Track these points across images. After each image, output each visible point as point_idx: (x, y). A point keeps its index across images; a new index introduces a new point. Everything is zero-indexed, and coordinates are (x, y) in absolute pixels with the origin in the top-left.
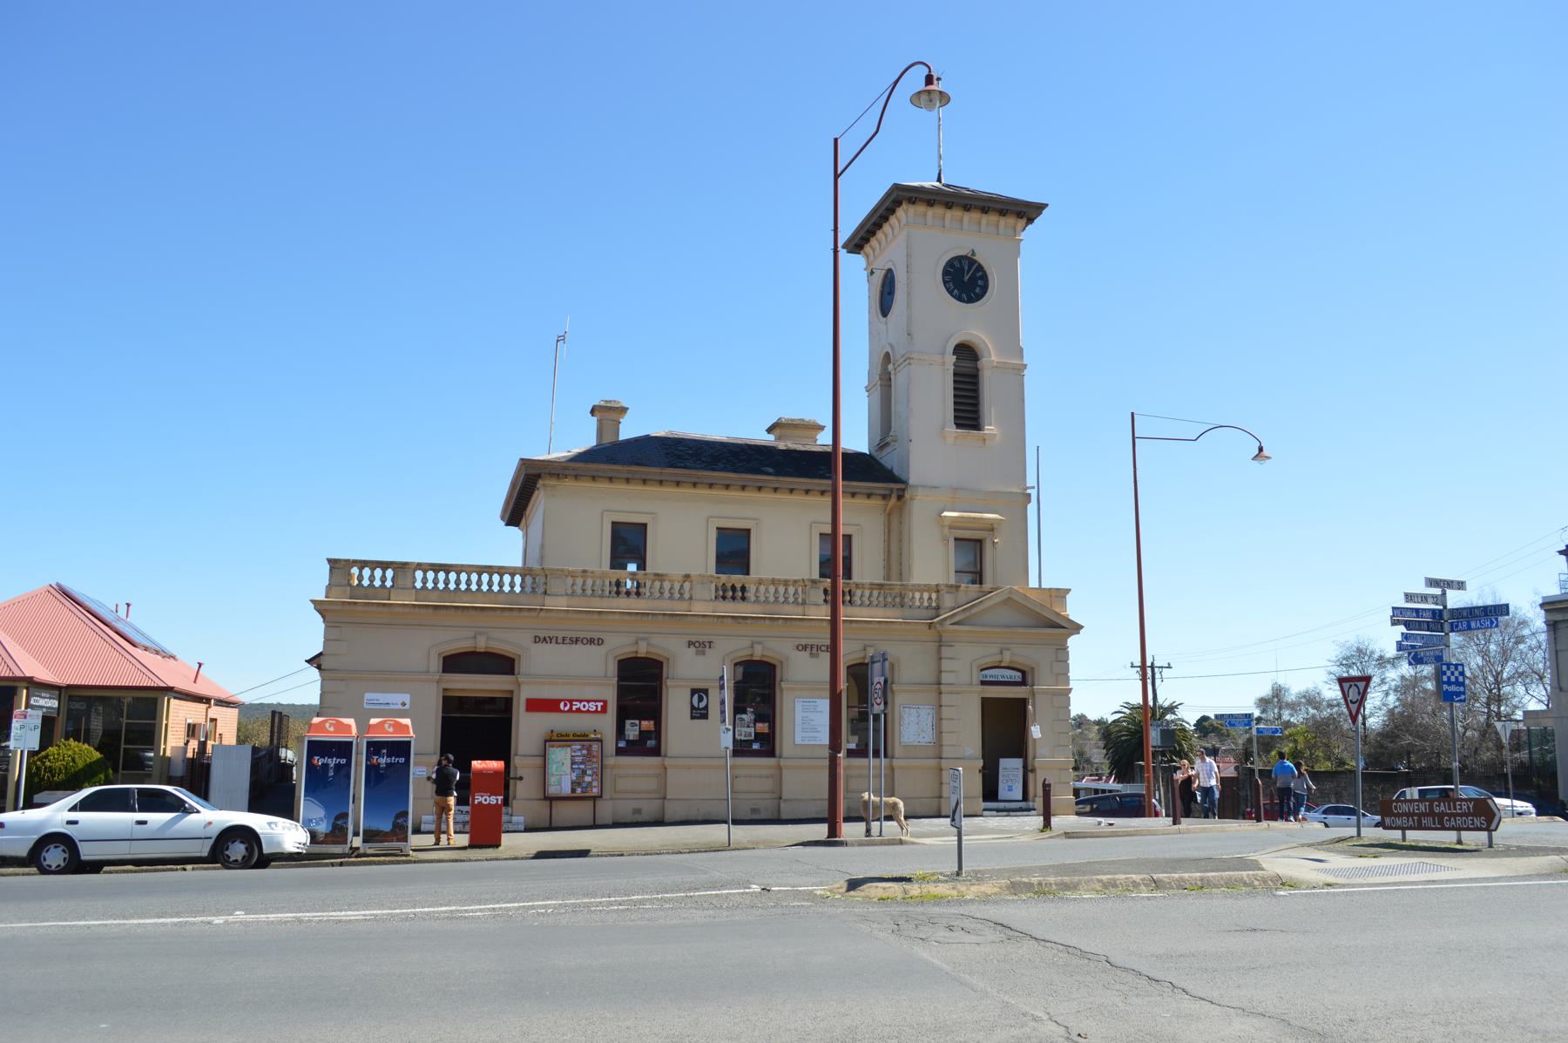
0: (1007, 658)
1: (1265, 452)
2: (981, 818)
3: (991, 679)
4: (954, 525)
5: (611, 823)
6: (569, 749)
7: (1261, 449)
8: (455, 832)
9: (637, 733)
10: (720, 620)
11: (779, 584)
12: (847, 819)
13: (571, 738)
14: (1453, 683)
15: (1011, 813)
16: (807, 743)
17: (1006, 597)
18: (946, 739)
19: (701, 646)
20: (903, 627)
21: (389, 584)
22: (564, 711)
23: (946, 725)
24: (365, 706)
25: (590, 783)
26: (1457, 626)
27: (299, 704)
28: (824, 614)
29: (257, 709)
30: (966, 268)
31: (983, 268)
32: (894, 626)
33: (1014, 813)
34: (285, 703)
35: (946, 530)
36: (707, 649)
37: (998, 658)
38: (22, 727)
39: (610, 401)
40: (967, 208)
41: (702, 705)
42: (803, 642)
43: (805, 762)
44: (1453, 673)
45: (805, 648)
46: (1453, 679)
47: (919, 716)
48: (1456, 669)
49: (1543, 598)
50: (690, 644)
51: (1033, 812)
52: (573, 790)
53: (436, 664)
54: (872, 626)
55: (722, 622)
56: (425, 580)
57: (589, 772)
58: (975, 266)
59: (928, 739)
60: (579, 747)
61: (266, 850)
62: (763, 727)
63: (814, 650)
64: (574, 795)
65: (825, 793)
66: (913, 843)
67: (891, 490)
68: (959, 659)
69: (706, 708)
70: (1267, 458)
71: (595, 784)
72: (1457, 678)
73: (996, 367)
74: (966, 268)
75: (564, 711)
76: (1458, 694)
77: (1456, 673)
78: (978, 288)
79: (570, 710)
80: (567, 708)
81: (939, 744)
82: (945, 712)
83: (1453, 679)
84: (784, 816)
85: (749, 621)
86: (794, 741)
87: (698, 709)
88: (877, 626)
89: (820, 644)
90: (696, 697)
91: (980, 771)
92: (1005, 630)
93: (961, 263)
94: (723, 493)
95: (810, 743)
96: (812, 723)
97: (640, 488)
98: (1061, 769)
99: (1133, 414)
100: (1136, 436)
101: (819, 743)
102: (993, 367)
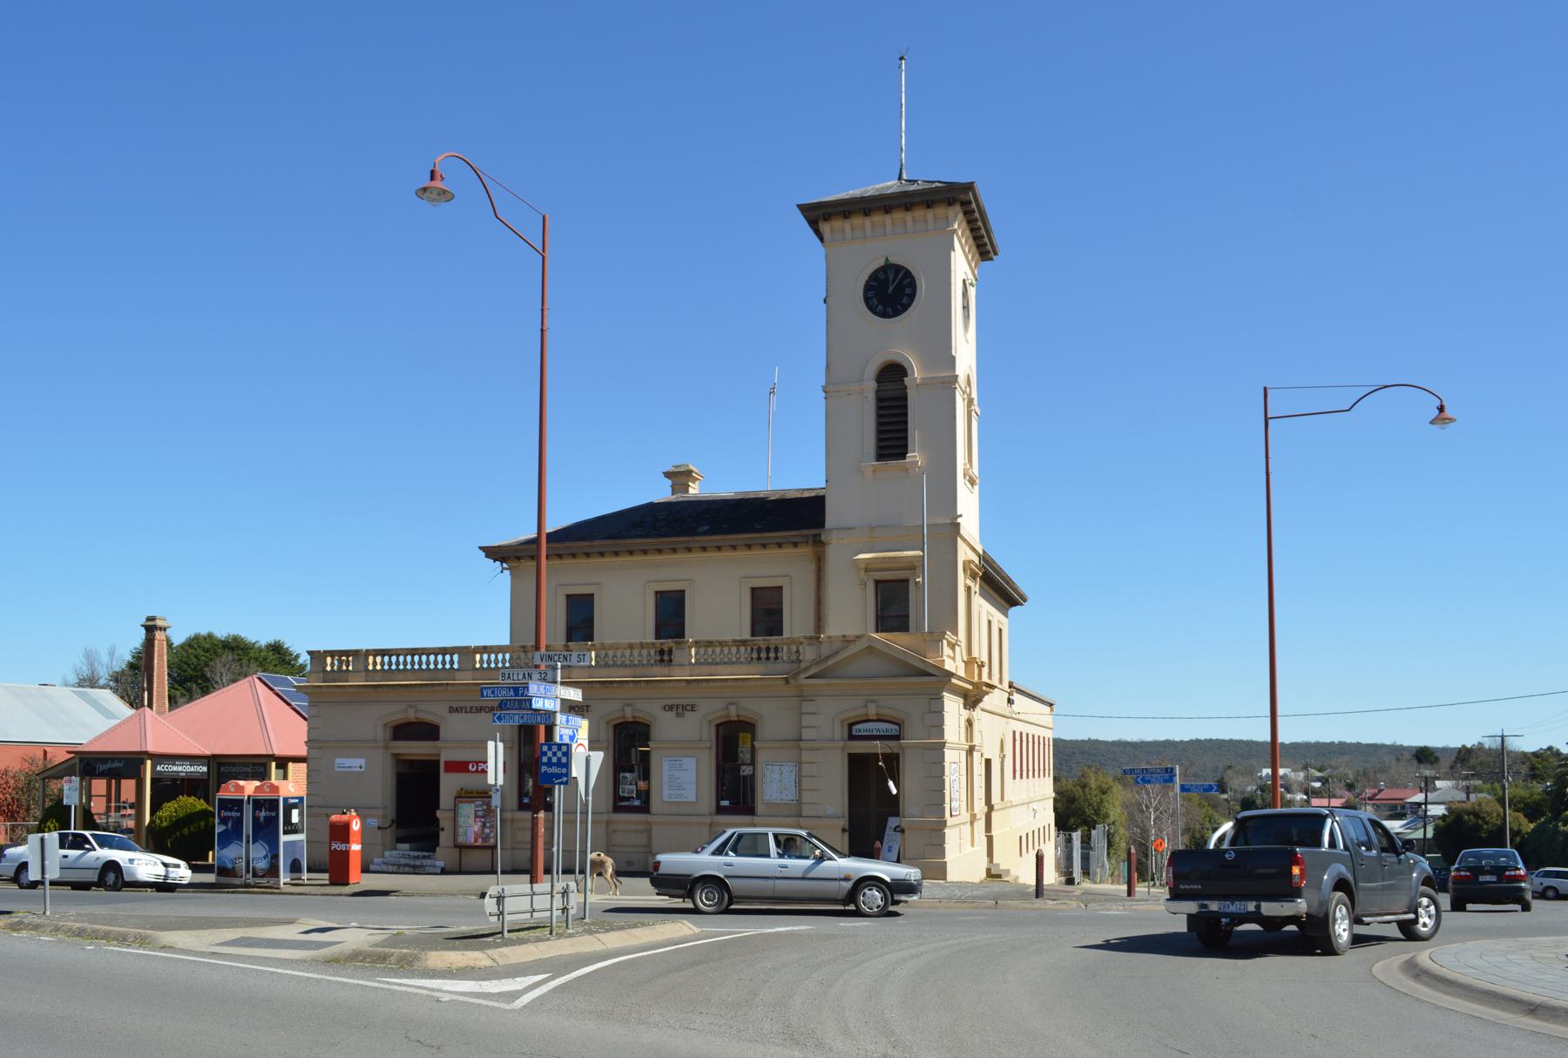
0: (872, 711)
1: (1448, 412)
3: (866, 733)
4: (869, 567)
6: (473, 805)
7: (1441, 409)
10: (590, 686)
13: (475, 795)
14: (554, 764)
16: (674, 800)
18: (806, 797)
20: (759, 683)
21: (456, 666)
22: (472, 772)
23: (806, 783)
24: (337, 769)
25: (488, 834)
26: (506, 704)
28: (688, 674)
30: (891, 278)
31: (910, 273)
32: (750, 683)
35: (862, 573)
37: (863, 711)
38: (70, 789)
39: (680, 466)
40: (867, 213)
42: (670, 702)
43: (670, 819)
44: (555, 754)
46: (554, 760)
52: (476, 840)
53: (381, 734)
54: (729, 684)
55: (592, 687)
56: (375, 663)
57: (488, 825)
58: (909, 280)
59: (790, 797)
60: (480, 803)
62: (642, 784)
63: (680, 710)
64: (476, 844)
65: (463, 856)
67: (807, 536)
68: (820, 714)
70: (1451, 420)
71: (492, 835)
72: (559, 759)
73: (923, 384)
74: (891, 278)
75: (472, 772)
76: (560, 776)
77: (559, 754)
78: (905, 298)
79: (477, 771)
80: (474, 769)
81: (799, 802)
82: (806, 770)
83: (554, 760)
85: (615, 685)
86: (662, 798)
88: (734, 683)
89: (685, 704)
91: (844, 830)
92: (865, 681)
93: (885, 273)
94: (657, 557)
95: (677, 800)
96: (679, 781)
97: (628, 558)
98: (934, 830)
99: (1265, 388)
100: (1269, 416)
101: (685, 800)
102: (917, 386)
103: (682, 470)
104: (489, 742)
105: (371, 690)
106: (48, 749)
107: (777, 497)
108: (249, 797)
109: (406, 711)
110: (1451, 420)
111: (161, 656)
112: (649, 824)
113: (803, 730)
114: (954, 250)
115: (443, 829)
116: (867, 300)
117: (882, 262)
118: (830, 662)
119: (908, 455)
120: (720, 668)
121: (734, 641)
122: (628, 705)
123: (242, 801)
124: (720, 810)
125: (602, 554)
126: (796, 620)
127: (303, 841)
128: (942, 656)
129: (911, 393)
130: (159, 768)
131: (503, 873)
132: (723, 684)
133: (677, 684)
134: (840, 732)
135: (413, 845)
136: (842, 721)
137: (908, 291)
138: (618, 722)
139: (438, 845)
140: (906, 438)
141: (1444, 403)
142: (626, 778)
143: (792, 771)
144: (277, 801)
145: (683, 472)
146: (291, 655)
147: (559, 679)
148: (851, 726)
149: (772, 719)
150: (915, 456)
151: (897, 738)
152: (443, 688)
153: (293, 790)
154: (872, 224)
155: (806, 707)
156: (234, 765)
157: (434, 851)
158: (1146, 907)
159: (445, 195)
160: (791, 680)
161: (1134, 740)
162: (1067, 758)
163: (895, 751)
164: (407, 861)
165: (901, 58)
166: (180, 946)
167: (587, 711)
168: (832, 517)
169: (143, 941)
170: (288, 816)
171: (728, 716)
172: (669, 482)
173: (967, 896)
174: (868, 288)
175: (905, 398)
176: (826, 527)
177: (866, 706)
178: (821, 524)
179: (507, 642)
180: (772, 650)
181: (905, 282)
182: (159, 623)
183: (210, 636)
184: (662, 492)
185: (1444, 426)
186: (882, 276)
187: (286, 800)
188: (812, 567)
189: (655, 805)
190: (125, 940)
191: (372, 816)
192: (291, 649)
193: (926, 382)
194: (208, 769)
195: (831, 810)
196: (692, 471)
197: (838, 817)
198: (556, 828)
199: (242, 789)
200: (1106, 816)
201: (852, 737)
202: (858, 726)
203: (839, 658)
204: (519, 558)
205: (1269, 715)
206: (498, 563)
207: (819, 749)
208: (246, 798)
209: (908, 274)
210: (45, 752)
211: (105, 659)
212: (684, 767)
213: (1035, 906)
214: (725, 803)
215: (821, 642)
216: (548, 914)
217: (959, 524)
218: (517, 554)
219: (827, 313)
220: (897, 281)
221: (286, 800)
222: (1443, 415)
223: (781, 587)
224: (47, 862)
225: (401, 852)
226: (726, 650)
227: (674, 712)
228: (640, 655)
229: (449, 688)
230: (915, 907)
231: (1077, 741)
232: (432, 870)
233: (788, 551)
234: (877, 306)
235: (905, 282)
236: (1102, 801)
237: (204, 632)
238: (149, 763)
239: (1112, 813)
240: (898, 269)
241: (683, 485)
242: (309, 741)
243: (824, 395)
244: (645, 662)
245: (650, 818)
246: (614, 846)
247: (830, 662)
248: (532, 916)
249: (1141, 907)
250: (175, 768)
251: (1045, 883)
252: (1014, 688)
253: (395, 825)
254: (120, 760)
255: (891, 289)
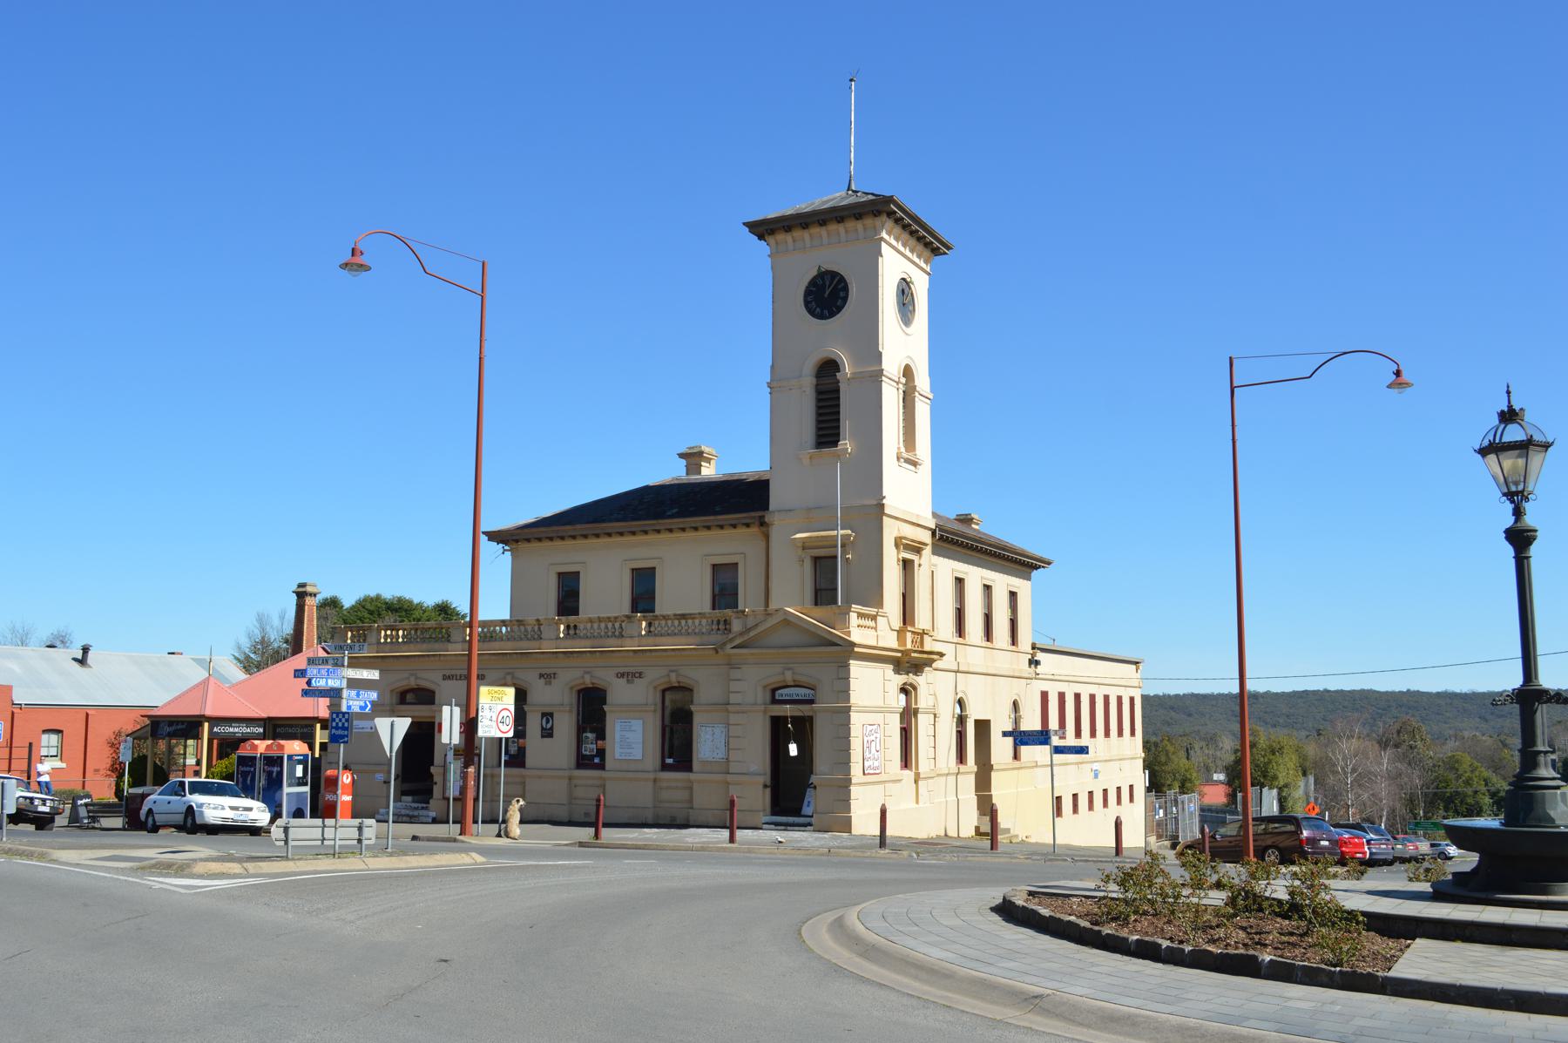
1: (1405, 376)
2: (761, 831)
4: (805, 545)
5: (567, 820)
7: (1398, 373)
8: (393, 822)
9: (516, 748)
11: (594, 622)
12: (738, 828)
15: (789, 828)
17: (782, 619)
18: (733, 756)
19: (548, 677)
20: (694, 653)
27: (1348, 689)
29: (1301, 697)
30: (827, 283)
33: (791, 828)
34: (1332, 689)
35: (800, 551)
36: (552, 680)
39: (693, 448)
41: (549, 726)
44: (340, 720)
45: (622, 675)
46: (340, 725)
47: (714, 734)
48: (344, 717)
49: (1029, 579)
50: (541, 676)
51: (809, 828)
54: (668, 654)
59: (721, 756)
61: (198, 821)
66: (463, 842)
69: (552, 728)
70: (1407, 385)
72: (343, 724)
73: (853, 378)
74: (827, 283)
76: (343, 737)
77: (343, 720)
83: (340, 725)
84: (691, 823)
87: (546, 729)
90: (545, 719)
91: (765, 786)
92: (781, 651)
93: (823, 280)
96: (628, 740)
97: (595, 541)
98: (840, 787)
99: (1230, 358)
100: (1235, 385)
103: (695, 451)
104: (444, 707)
105: (380, 660)
106: (89, 712)
107: (756, 478)
108: (261, 754)
109: (408, 678)
110: (1407, 385)
111: (311, 621)
112: (604, 779)
113: (731, 695)
114: (882, 256)
115: (436, 783)
116: (807, 304)
117: (814, 273)
118: (752, 634)
119: (840, 443)
120: (664, 639)
121: (675, 615)
122: (588, 673)
123: (255, 757)
124: (665, 767)
125: (585, 536)
126: (748, 598)
127: (307, 792)
128: (849, 628)
129: (843, 387)
130: (215, 730)
131: (483, 822)
132: (664, 654)
133: (626, 654)
134: (762, 696)
135: (416, 798)
136: (765, 687)
137: (842, 294)
138: (579, 688)
139: (432, 797)
140: (839, 427)
141: (1401, 368)
142: (587, 737)
143: (722, 732)
144: (282, 758)
145: (695, 453)
146: (459, 615)
147: (346, 664)
148: (774, 691)
149: (707, 690)
150: (846, 444)
151: (811, 702)
152: (437, 658)
153: (298, 748)
154: (810, 235)
155: (735, 674)
156: (291, 726)
157: (428, 803)
158: (983, 859)
159: (363, 267)
160: (719, 650)
161: (1463, 692)
162: (1380, 711)
163: (810, 714)
164: (407, 812)
165: (851, 80)
166: (63, 860)
167: (554, 678)
168: (776, 498)
169: (42, 857)
170: (292, 771)
171: (670, 682)
172: (683, 462)
173: (863, 844)
174: (808, 293)
175: (837, 391)
176: (771, 509)
177: (783, 674)
178: (765, 505)
179: (507, 617)
180: (722, 623)
181: (840, 287)
182: (309, 589)
183: (378, 597)
184: (671, 471)
185: (1400, 390)
186: (820, 282)
187: (290, 757)
188: (763, 544)
189: (609, 764)
190: (32, 856)
191: (380, 772)
192: (458, 609)
193: (856, 377)
194: (264, 730)
195: (754, 768)
196: (703, 452)
197: (760, 775)
198: (703, 787)
199: (255, 747)
200: (1275, 778)
201: (774, 701)
202: (780, 691)
203: (760, 629)
204: (517, 541)
205: (1238, 677)
206: (501, 545)
207: (743, 712)
208: (259, 755)
209: (842, 279)
210: (87, 714)
211: (276, 622)
212: (633, 729)
213: (866, 855)
214: (670, 761)
215: (746, 616)
216: (332, 842)
217: (883, 504)
218: (514, 538)
219: (773, 317)
220: (833, 286)
221: (290, 757)
222: (1400, 380)
223: (737, 564)
224: (5, 801)
225: (404, 804)
226: (670, 622)
227: (625, 679)
228: (599, 627)
229: (442, 658)
230: (754, 853)
231: (1393, 693)
232: (425, 820)
233: (742, 531)
234: (815, 309)
235: (840, 287)
236: (1270, 761)
237: (373, 594)
238: (206, 725)
239: (1280, 775)
240: (834, 274)
241: (697, 464)
242: (331, 705)
243: (769, 390)
244: (603, 633)
245: (691, 776)
246: (575, 799)
247: (752, 634)
248: (323, 843)
249: (976, 859)
250: (231, 730)
251: (1124, 846)
252: (1039, 649)
253: (400, 779)
254: (183, 723)
255: (827, 293)
